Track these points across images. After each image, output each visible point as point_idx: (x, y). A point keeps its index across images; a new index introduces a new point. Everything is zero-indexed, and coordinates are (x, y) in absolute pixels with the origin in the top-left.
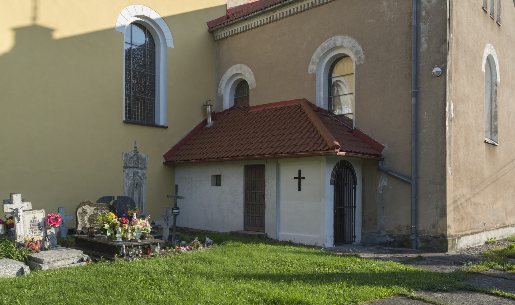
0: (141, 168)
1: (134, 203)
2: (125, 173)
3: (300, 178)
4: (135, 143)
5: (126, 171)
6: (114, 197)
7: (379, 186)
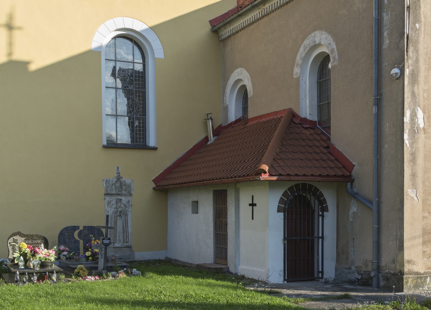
0: (125, 195)
2: (106, 201)
3: (253, 205)
4: (118, 168)
5: (108, 198)
6: (78, 227)
7: (350, 213)
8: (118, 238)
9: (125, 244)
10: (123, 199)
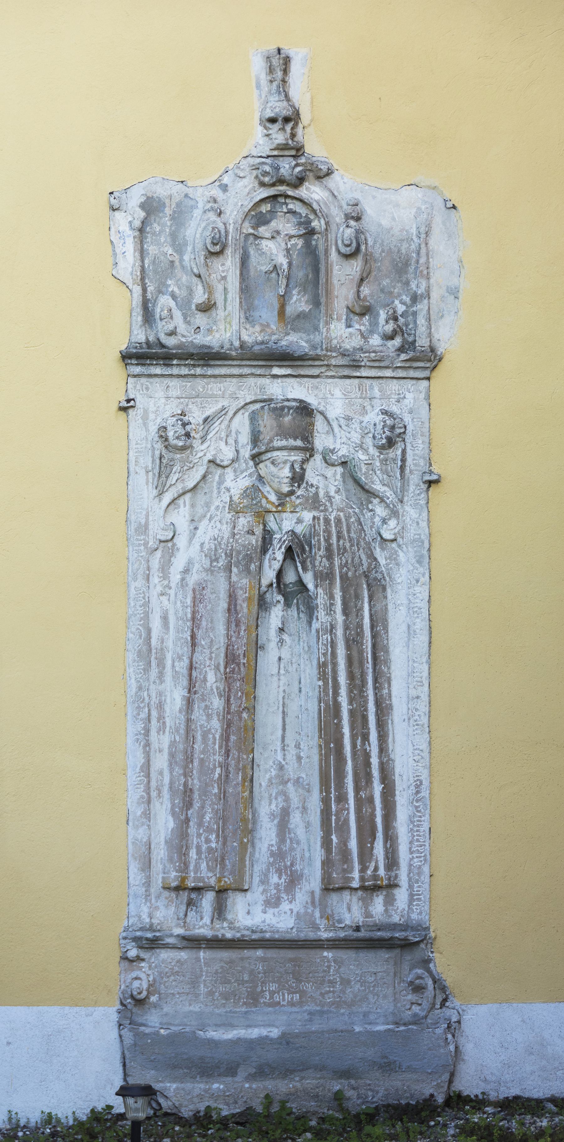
0: (352, 365)
1: (219, 476)
4: (280, 64)
5: (162, 398)
8: (267, 835)
9: (350, 911)
10: (336, 409)
